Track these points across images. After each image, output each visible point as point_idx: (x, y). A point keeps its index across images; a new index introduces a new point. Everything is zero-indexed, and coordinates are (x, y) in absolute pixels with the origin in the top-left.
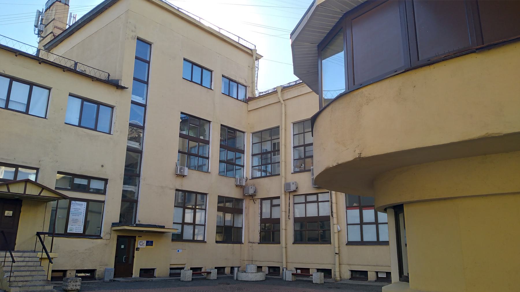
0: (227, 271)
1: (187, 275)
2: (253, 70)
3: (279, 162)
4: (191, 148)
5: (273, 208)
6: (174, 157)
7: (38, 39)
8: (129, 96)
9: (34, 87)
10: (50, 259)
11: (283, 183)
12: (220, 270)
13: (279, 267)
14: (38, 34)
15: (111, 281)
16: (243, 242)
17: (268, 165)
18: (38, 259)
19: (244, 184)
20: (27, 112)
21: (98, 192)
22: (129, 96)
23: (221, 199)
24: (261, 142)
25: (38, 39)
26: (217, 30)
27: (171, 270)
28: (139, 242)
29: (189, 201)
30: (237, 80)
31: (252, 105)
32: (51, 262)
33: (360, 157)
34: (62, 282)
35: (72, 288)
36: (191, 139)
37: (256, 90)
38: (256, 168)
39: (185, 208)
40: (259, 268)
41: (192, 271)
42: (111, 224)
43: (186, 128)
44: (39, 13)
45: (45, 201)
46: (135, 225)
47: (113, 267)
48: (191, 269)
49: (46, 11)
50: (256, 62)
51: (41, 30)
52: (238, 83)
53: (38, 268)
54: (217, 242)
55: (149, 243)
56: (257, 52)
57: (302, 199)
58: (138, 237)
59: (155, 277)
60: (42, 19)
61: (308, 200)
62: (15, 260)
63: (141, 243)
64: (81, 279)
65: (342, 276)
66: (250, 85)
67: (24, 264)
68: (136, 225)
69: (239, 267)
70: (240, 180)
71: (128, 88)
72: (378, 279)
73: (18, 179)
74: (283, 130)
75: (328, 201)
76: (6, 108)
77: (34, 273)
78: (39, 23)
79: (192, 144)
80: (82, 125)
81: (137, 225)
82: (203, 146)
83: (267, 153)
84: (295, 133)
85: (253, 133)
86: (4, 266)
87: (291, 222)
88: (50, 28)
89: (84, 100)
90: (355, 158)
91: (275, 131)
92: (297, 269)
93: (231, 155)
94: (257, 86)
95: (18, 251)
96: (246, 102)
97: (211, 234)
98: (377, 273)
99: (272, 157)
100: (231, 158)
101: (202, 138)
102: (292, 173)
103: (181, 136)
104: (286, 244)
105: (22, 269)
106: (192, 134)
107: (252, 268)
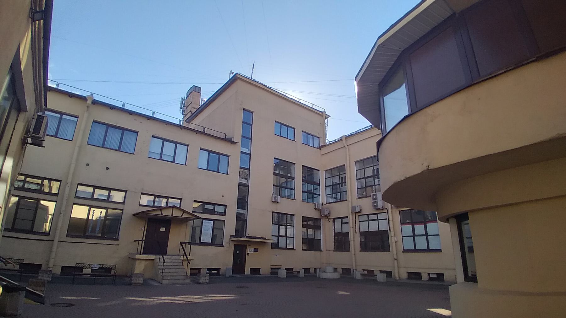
0: (312, 271)
1: (283, 273)
2: (323, 126)
3: (346, 191)
4: (282, 183)
5: (343, 225)
6: (271, 189)
7: (183, 116)
8: (239, 148)
9: (178, 145)
10: (189, 261)
11: (350, 206)
12: (307, 270)
13: (350, 269)
14: (182, 113)
15: (230, 276)
16: (322, 250)
17: (338, 194)
18: (181, 261)
19: (321, 208)
20: (173, 162)
21: (220, 214)
22: (239, 148)
23: (305, 219)
24: (332, 177)
25: (183, 116)
26: (298, 100)
27: (192, 270)
28: (249, 249)
29: (282, 220)
30: (313, 133)
31: (324, 150)
32: (189, 263)
33: (428, 169)
34: (196, 277)
35: (202, 282)
36: (281, 176)
37: (326, 140)
38: (329, 195)
39: (279, 225)
40: (335, 269)
41: (286, 270)
42: (230, 236)
43: (277, 169)
44: (183, 99)
45: (186, 221)
46: (246, 237)
47: (232, 267)
48: (286, 269)
49: (187, 97)
50: (326, 120)
51: (184, 110)
52: (313, 136)
53: (181, 267)
54: (303, 250)
55: (256, 250)
56: (326, 113)
57: (365, 218)
58: (248, 245)
59: (261, 274)
60: (184, 103)
61: (370, 219)
62: (165, 261)
63: (250, 250)
64: (209, 275)
65: (400, 276)
66: (322, 137)
67: (172, 264)
68: (247, 237)
69: (320, 268)
70: (318, 205)
71: (238, 143)
72: (431, 279)
73: (168, 206)
74: (348, 167)
75: (386, 219)
76: (161, 159)
77: (177, 270)
78: (183, 106)
79: (283, 180)
80: (209, 169)
81: (247, 237)
82: (290, 181)
83: (337, 184)
84: (357, 169)
85: (326, 171)
86: (159, 265)
87: (358, 235)
88: (189, 109)
89: (210, 152)
90: (423, 170)
91: (342, 168)
92: (364, 270)
93: (310, 187)
94: (327, 137)
95: (168, 255)
96: (319, 149)
97: (298, 244)
98: (429, 274)
99: (341, 188)
100: (310, 189)
101: (289, 175)
102: (356, 199)
103: (275, 174)
104: (355, 252)
105: (170, 267)
106: (282, 173)
107: (330, 269)
